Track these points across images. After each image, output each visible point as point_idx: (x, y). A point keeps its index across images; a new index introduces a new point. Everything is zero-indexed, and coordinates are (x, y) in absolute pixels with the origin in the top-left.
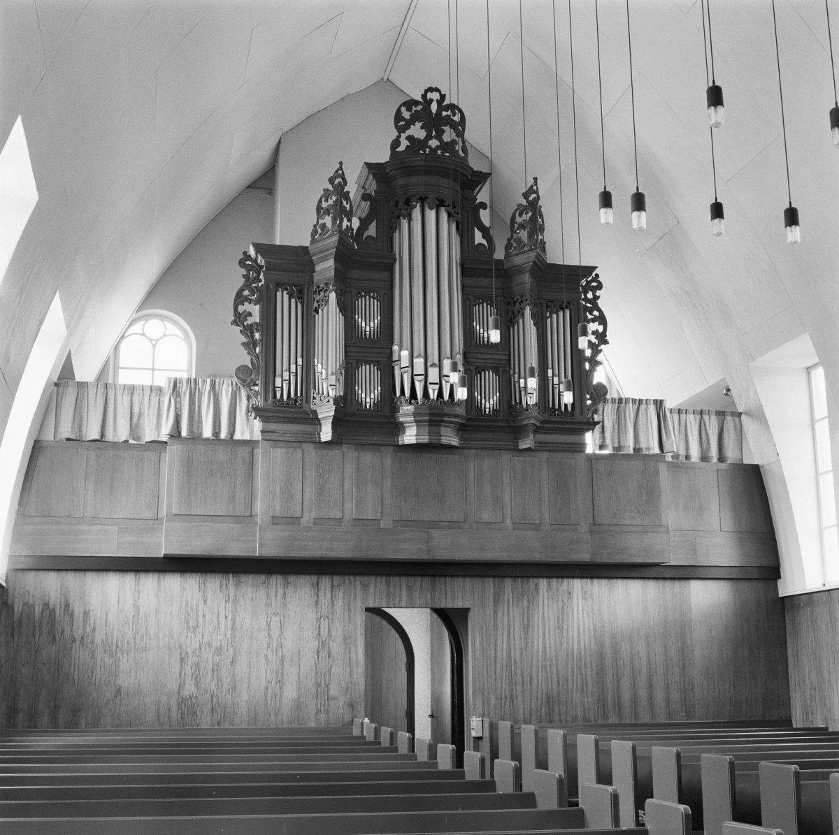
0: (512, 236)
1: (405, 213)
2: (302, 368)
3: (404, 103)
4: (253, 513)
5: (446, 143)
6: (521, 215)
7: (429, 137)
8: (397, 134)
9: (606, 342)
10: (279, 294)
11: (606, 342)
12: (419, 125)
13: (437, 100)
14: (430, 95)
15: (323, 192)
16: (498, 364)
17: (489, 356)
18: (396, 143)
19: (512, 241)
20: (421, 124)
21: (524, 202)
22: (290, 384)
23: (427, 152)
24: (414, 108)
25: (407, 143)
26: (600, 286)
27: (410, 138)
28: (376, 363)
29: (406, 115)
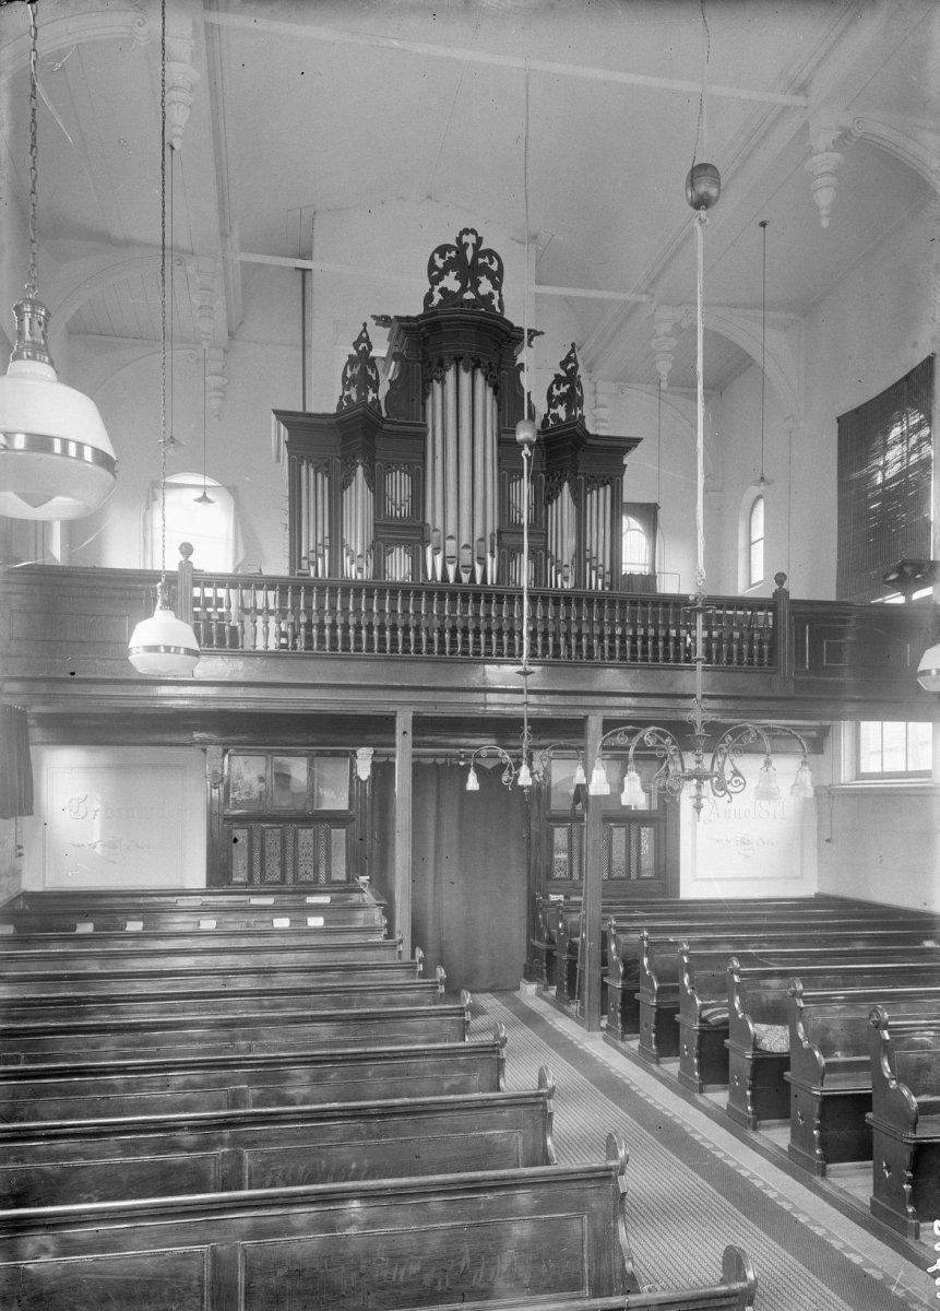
6: (558, 388)
7: (463, 289)
10: (304, 468)
14: (465, 239)
18: (429, 298)
27: (443, 291)
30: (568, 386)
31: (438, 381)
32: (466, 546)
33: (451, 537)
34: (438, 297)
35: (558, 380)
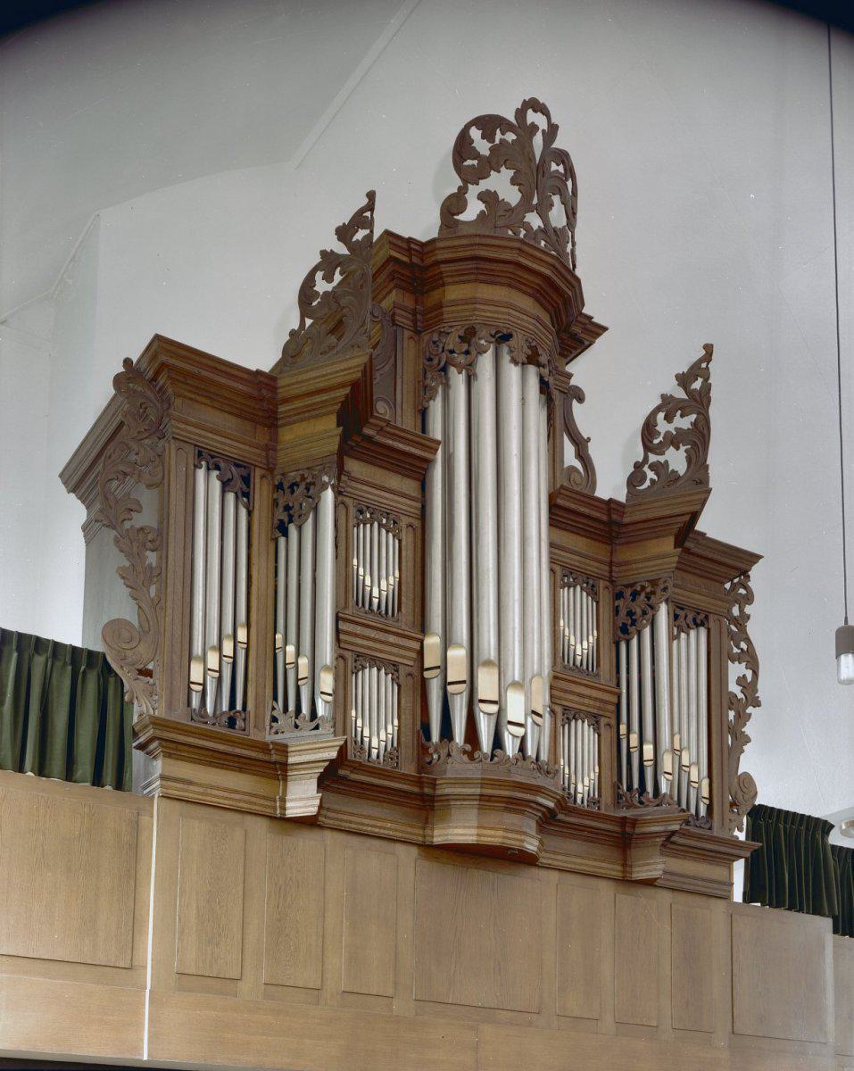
0: (646, 459)
1: (461, 359)
2: (247, 650)
3: (477, 118)
4: (135, 963)
5: (555, 230)
6: (669, 418)
7: (526, 205)
8: (460, 183)
9: (757, 704)
10: (201, 474)
11: (757, 704)
12: (507, 174)
13: (543, 131)
14: (533, 117)
15: (318, 259)
16: (599, 708)
17: (386, 797)
18: (452, 206)
19: (646, 469)
20: (511, 173)
21: (681, 394)
22: (220, 680)
23: (522, 236)
24: (498, 136)
25: (481, 206)
26: (749, 598)
27: (488, 197)
28: (393, 668)
29: (483, 147)
30: (693, 417)
31: (460, 369)
32: (516, 685)
33: (488, 663)
34: (473, 210)
35: (669, 406)
